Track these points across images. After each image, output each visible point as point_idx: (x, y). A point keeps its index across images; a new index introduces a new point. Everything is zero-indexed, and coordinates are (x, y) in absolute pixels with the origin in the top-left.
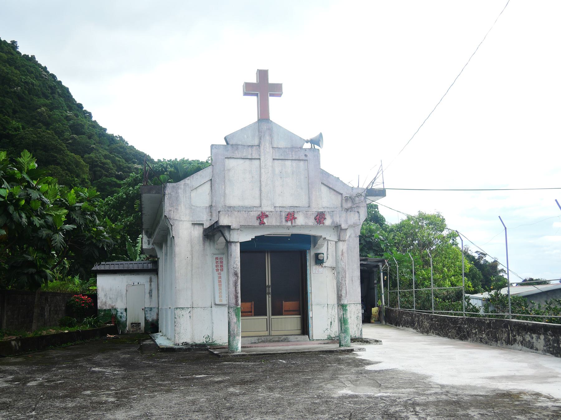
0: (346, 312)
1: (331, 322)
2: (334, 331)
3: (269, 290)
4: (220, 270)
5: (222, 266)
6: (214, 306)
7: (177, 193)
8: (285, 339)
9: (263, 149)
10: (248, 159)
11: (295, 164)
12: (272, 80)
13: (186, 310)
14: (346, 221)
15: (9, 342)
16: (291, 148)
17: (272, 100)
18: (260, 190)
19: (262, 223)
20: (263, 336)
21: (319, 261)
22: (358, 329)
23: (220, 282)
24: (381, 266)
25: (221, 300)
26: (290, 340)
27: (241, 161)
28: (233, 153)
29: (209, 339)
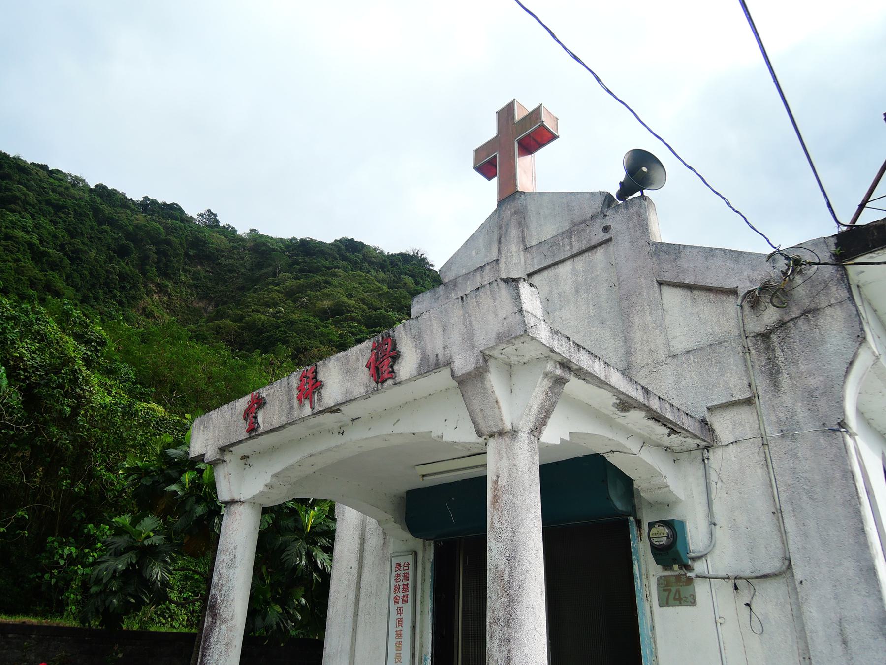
11: (581, 264)
14: (469, 338)
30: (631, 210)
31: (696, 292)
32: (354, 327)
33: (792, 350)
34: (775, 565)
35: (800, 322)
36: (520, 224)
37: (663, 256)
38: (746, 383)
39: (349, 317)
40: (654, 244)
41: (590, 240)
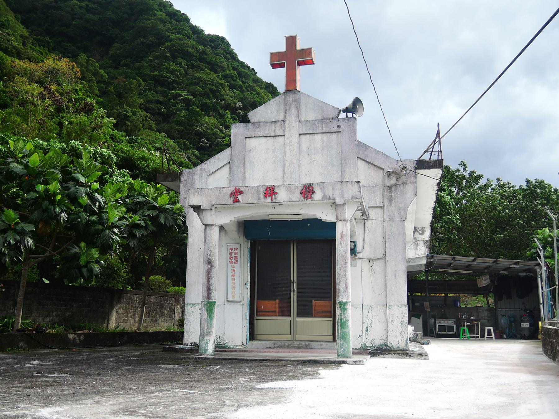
0: (344, 311)
1: (367, 328)
2: (370, 339)
3: (294, 287)
4: (233, 263)
5: (236, 258)
6: (227, 303)
7: (193, 179)
8: (307, 346)
9: (288, 124)
10: (271, 136)
12: (300, 46)
13: (197, 306)
14: (342, 195)
16: (322, 119)
18: (284, 171)
19: (236, 201)
22: (403, 337)
23: (233, 275)
25: (233, 297)
26: (312, 347)
27: (263, 140)
28: (254, 131)
29: (220, 340)
30: (350, 123)
31: (370, 165)
33: (397, 194)
35: (401, 186)
36: (297, 107)
37: (361, 147)
38: (382, 201)
40: (358, 141)
41: (331, 129)
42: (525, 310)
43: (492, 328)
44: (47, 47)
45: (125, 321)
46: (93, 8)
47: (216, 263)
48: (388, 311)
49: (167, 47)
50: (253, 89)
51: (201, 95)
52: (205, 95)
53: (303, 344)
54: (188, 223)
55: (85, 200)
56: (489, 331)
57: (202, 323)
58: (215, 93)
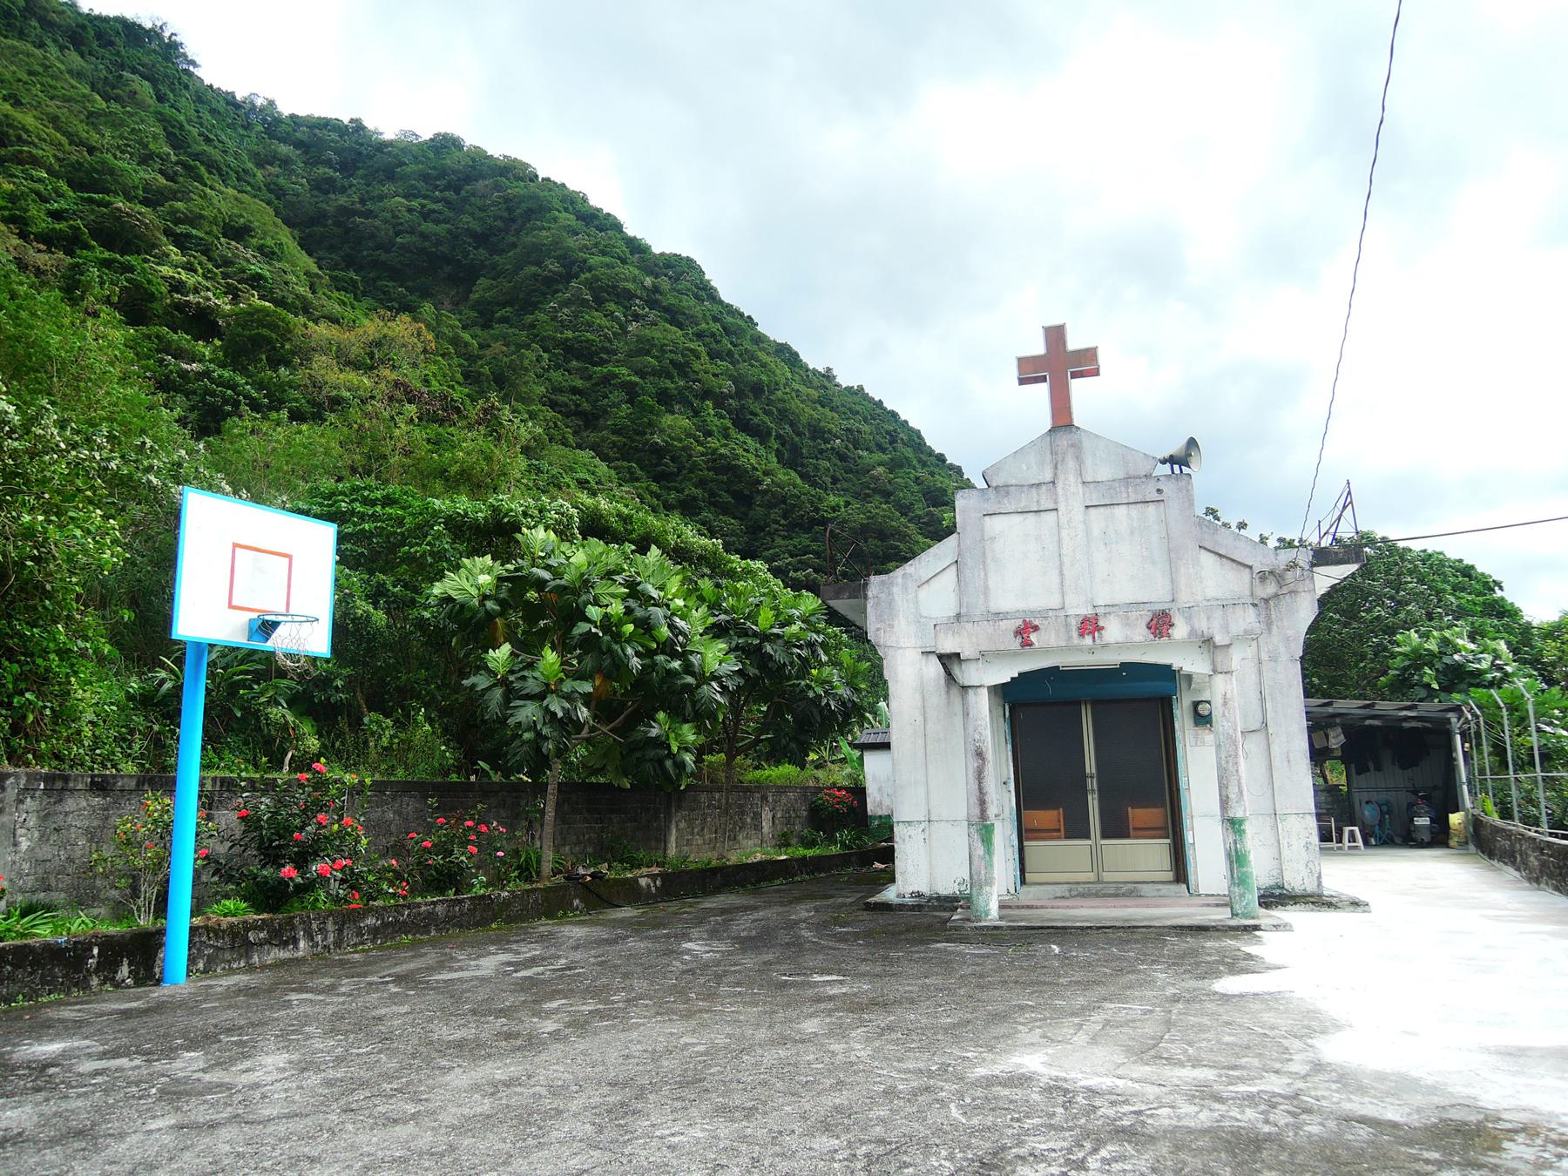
0: (1240, 836)
3: (1092, 784)
12: (1074, 343)
14: (1225, 628)
15: (635, 880)
17: (1078, 387)
18: (1061, 574)
19: (1027, 644)
20: (1084, 883)
21: (1202, 719)
24: (1454, 720)
32: (40, 180)
34: (1257, 725)
36: (1077, 458)
37: (1205, 529)
39: (25, 155)
42: (1415, 792)
43: (1356, 829)
44: (351, 292)
45: (689, 843)
46: (434, 211)
47: (989, 756)
48: (1280, 825)
49: (587, 283)
50: (753, 357)
51: (654, 373)
52: (664, 373)
53: (1125, 888)
54: (886, 675)
55: (665, 631)
56: (1352, 834)
57: (976, 863)
58: (683, 369)
